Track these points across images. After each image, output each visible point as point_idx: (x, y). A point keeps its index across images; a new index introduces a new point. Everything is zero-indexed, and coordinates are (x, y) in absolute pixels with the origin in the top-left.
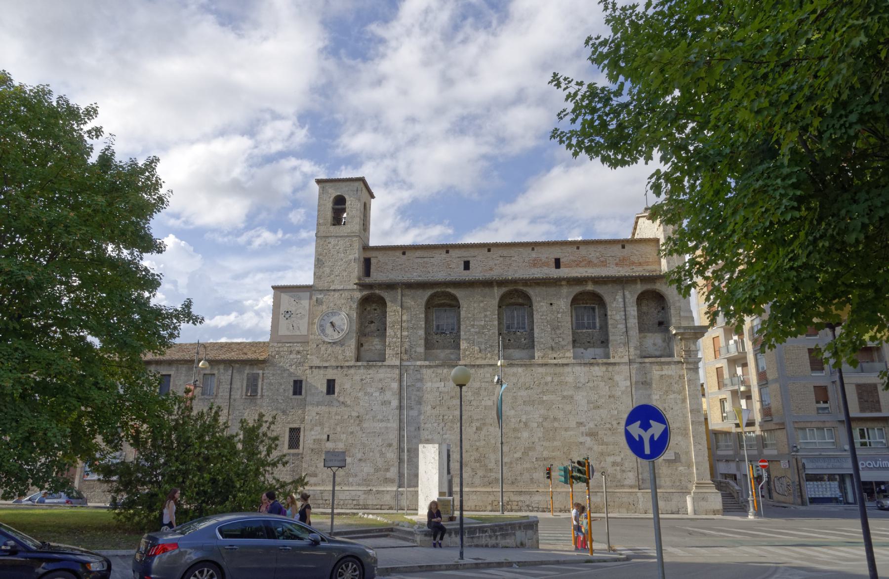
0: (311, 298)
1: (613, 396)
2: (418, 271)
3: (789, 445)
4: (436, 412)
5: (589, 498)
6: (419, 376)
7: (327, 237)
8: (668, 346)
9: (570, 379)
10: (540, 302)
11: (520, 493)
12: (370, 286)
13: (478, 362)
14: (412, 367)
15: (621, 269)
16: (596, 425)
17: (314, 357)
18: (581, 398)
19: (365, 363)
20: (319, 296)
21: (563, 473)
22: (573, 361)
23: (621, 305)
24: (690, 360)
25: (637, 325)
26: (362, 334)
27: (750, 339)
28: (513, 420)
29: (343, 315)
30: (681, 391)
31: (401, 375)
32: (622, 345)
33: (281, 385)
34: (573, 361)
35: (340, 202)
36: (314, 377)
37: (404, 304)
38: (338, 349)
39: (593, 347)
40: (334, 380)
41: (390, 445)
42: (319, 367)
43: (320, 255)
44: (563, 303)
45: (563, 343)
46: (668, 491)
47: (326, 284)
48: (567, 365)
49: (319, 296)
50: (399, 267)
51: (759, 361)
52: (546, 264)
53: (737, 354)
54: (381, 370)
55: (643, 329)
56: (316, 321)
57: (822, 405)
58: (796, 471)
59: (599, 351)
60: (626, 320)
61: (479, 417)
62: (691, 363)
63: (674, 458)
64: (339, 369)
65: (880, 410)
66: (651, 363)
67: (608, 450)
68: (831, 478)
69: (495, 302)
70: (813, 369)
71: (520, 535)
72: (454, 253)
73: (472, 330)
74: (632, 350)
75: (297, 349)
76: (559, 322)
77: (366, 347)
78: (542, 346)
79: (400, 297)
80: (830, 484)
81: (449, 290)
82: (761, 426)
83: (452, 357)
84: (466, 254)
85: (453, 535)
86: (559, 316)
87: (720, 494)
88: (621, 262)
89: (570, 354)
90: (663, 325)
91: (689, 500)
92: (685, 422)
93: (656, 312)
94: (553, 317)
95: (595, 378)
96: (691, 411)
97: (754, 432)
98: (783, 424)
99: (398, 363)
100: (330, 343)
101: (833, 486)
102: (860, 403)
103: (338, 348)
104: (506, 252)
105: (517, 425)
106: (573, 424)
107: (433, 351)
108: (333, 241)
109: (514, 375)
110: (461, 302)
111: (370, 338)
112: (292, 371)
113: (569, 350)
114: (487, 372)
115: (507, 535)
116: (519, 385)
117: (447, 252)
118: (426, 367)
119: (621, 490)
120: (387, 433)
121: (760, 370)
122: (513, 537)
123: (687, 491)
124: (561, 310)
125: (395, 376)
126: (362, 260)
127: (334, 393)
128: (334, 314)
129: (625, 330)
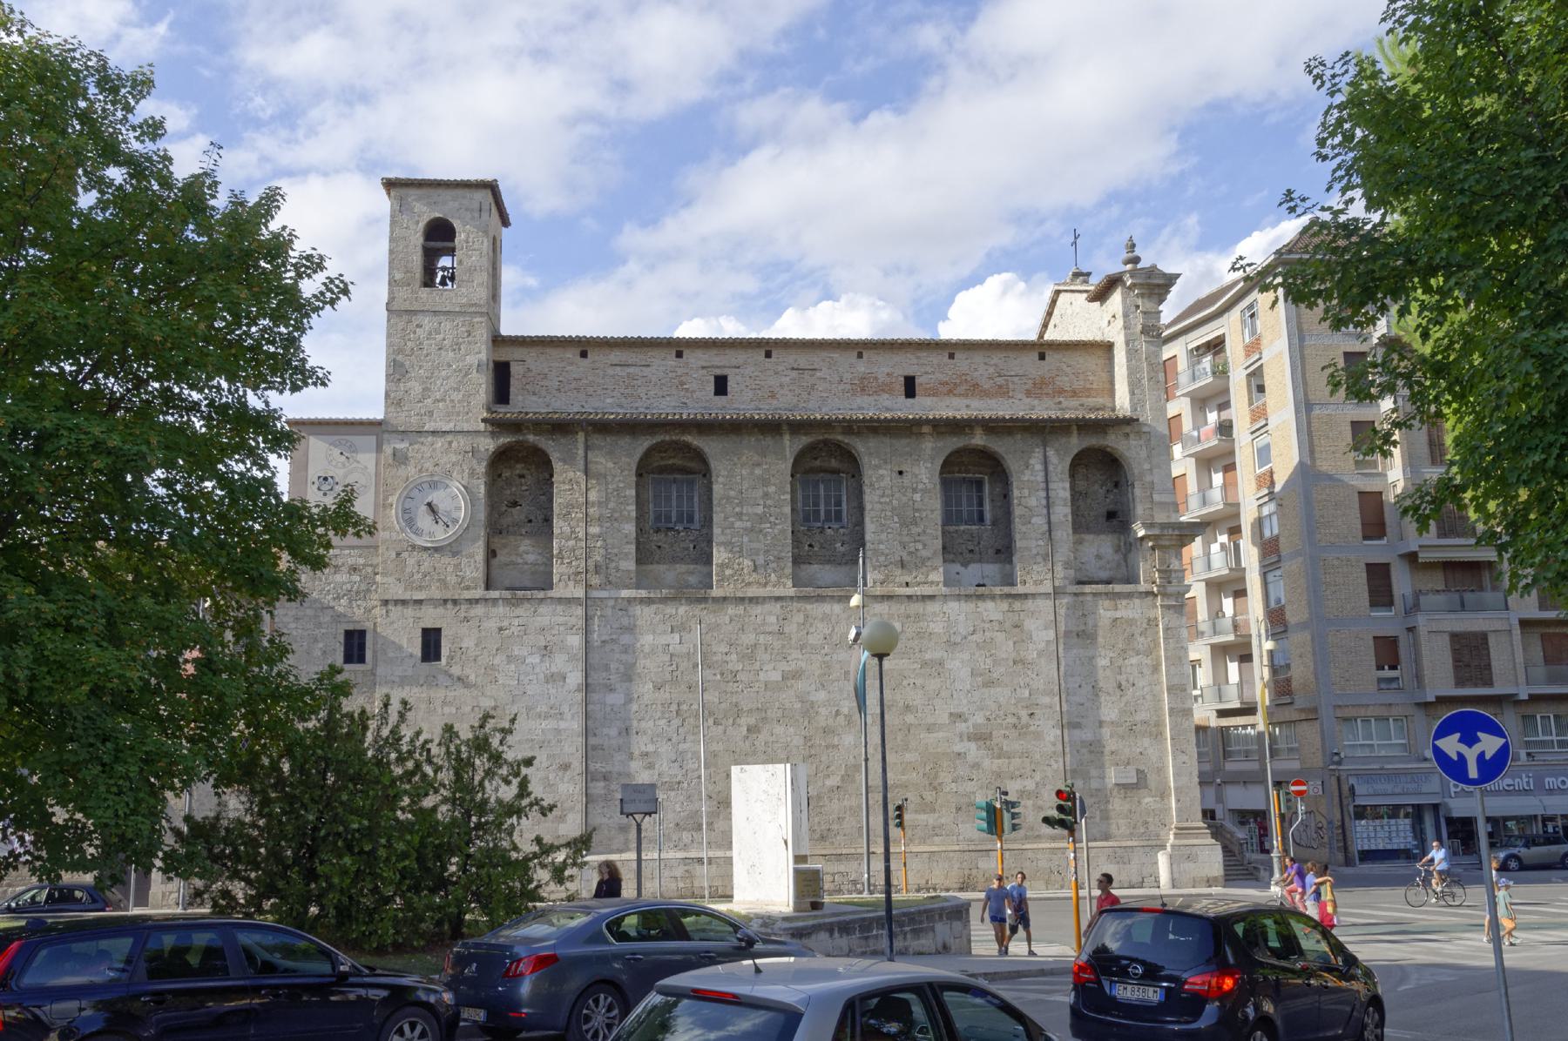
0: (379, 449)
1: (1022, 662)
2: (615, 394)
3: (1324, 751)
4: (664, 695)
5: (1075, 858)
6: (625, 621)
7: (415, 312)
8: (1126, 561)
9: (937, 627)
10: (878, 467)
11: (839, 857)
12: (515, 426)
13: (752, 592)
14: (611, 603)
15: (1036, 402)
16: (989, 719)
17: (391, 580)
18: (958, 665)
19: (507, 594)
20: (401, 446)
21: (984, 814)
22: (944, 590)
23: (1040, 477)
24: (1171, 589)
25: (1070, 518)
26: (496, 529)
27: (1254, 543)
28: (823, 711)
29: (456, 487)
30: (1151, 650)
31: (588, 618)
32: (1039, 559)
33: (316, 640)
34: (944, 590)
35: (440, 235)
36: (392, 623)
37: (592, 467)
38: (446, 560)
39: (980, 561)
40: (438, 631)
41: (566, 767)
42: (404, 602)
43: (400, 351)
44: (925, 472)
45: (925, 553)
46: (1124, 844)
47: (414, 420)
48: (932, 597)
49: (401, 446)
50: (574, 385)
51: (1271, 587)
52: (886, 388)
53: (1227, 572)
54: (543, 609)
55: (1080, 525)
56: (393, 499)
57: (1388, 673)
58: (1336, 800)
59: (991, 569)
60: (1048, 507)
61: (754, 706)
62: (1171, 595)
63: (1135, 781)
64: (449, 606)
65: (1490, 683)
66: (1095, 594)
67: (1012, 768)
68: (1394, 811)
69: (786, 466)
70: (1374, 604)
71: (942, 929)
72: (693, 358)
73: (738, 524)
74: (1059, 568)
75: (351, 561)
76: (917, 510)
77: (502, 557)
78: (882, 559)
79: (581, 452)
80: (1397, 825)
81: (688, 438)
82: (1270, 713)
83: (692, 580)
84: (721, 362)
85: (836, 934)
86: (917, 497)
87: (1219, 848)
88: (1039, 388)
89: (937, 576)
90: (1117, 519)
91: (1162, 860)
92: (1158, 709)
93: (1102, 491)
94: (904, 499)
95: (987, 626)
96: (1169, 690)
97: (1253, 726)
98: (1315, 710)
99: (579, 592)
100: (426, 549)
101: (1401, 828)
102: (1456, 668)
103: (445, 560)
104: (803, 360)
105: (830, 722)
106: (945, 719)
107: (650, 567)
108: (427, 322)
109: (826, 618)
110: (713, 464)
111: (512, 538)
112: (341, 609)
113: (936, 568)
114: (770, 613)
115: (921, 930)
116: (836, 639)
117: (679, 355)
118: (642, 601)
119: (1035, 846)
120: (559, 741)
121: (1273, 605)
122: (931, 934)
123: (1159, 843)
124: (921, 486)
125: (573, 621)
126: (491, 365)
127: (438, 657)
128: (434, 485)
129: (1045, 527)
